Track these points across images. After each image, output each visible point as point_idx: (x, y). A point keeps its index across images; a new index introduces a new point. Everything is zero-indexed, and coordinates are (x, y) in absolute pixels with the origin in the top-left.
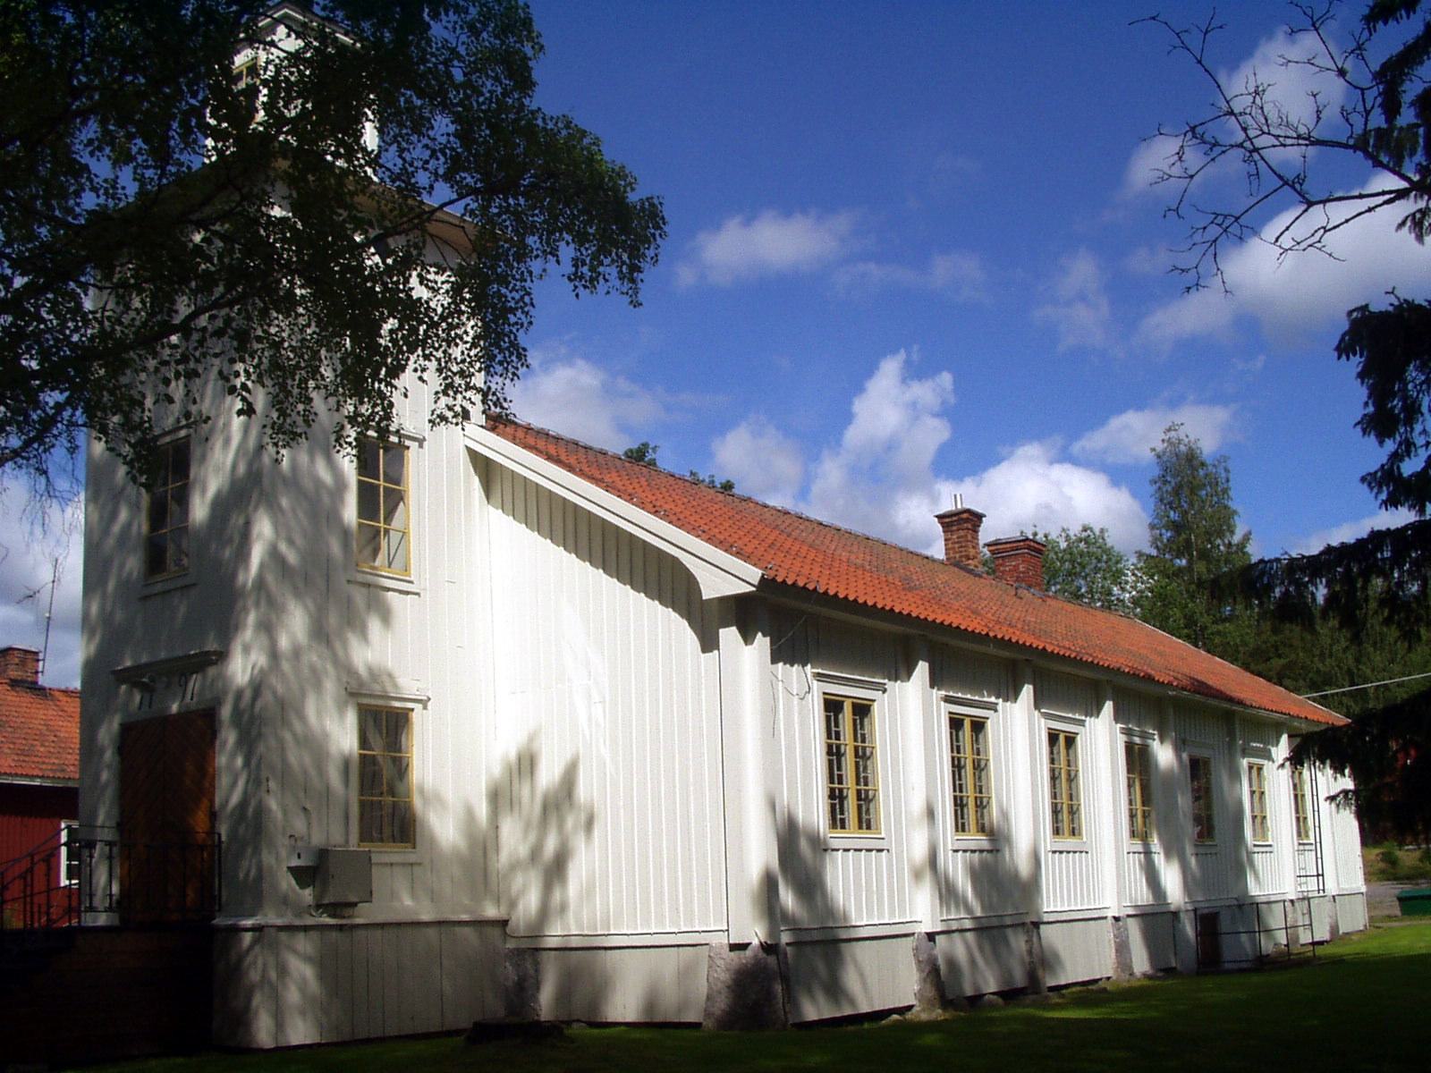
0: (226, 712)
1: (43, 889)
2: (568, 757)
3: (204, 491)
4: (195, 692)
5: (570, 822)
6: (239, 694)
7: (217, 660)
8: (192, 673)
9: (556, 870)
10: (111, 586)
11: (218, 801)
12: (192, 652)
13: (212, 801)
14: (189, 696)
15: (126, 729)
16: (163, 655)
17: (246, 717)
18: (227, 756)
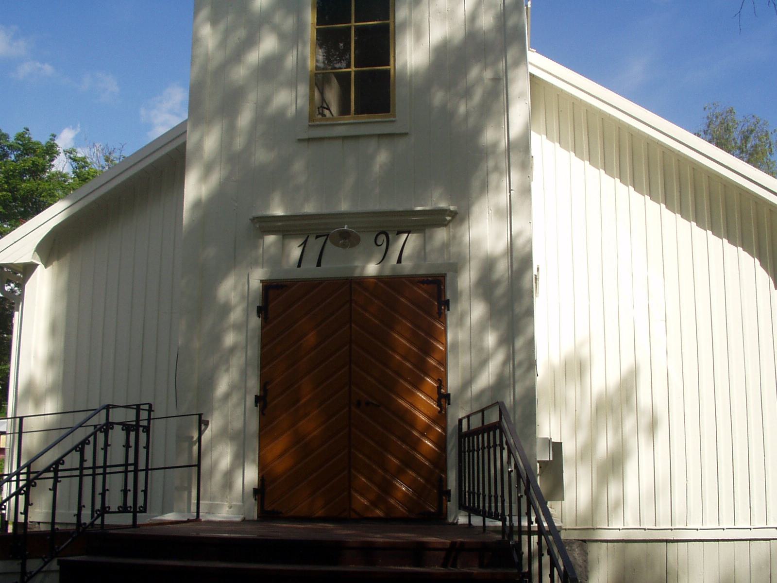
0: (467, 279)
1: (129, 473)
2: (627, 364)
3: (419, 36)
4: (406, 253)
5: (629, 424)
6: (489, 265)
7: (450, 221)
8: (400, 233)
9: (613, 466)
10: (245, 119)
11: (453, 381)
12: (419, 208)
13: (442, 382)
14: (394, 260)
15: (270, 288)
16: (344, 207)
17: (500, 291)
18: (468, 327)
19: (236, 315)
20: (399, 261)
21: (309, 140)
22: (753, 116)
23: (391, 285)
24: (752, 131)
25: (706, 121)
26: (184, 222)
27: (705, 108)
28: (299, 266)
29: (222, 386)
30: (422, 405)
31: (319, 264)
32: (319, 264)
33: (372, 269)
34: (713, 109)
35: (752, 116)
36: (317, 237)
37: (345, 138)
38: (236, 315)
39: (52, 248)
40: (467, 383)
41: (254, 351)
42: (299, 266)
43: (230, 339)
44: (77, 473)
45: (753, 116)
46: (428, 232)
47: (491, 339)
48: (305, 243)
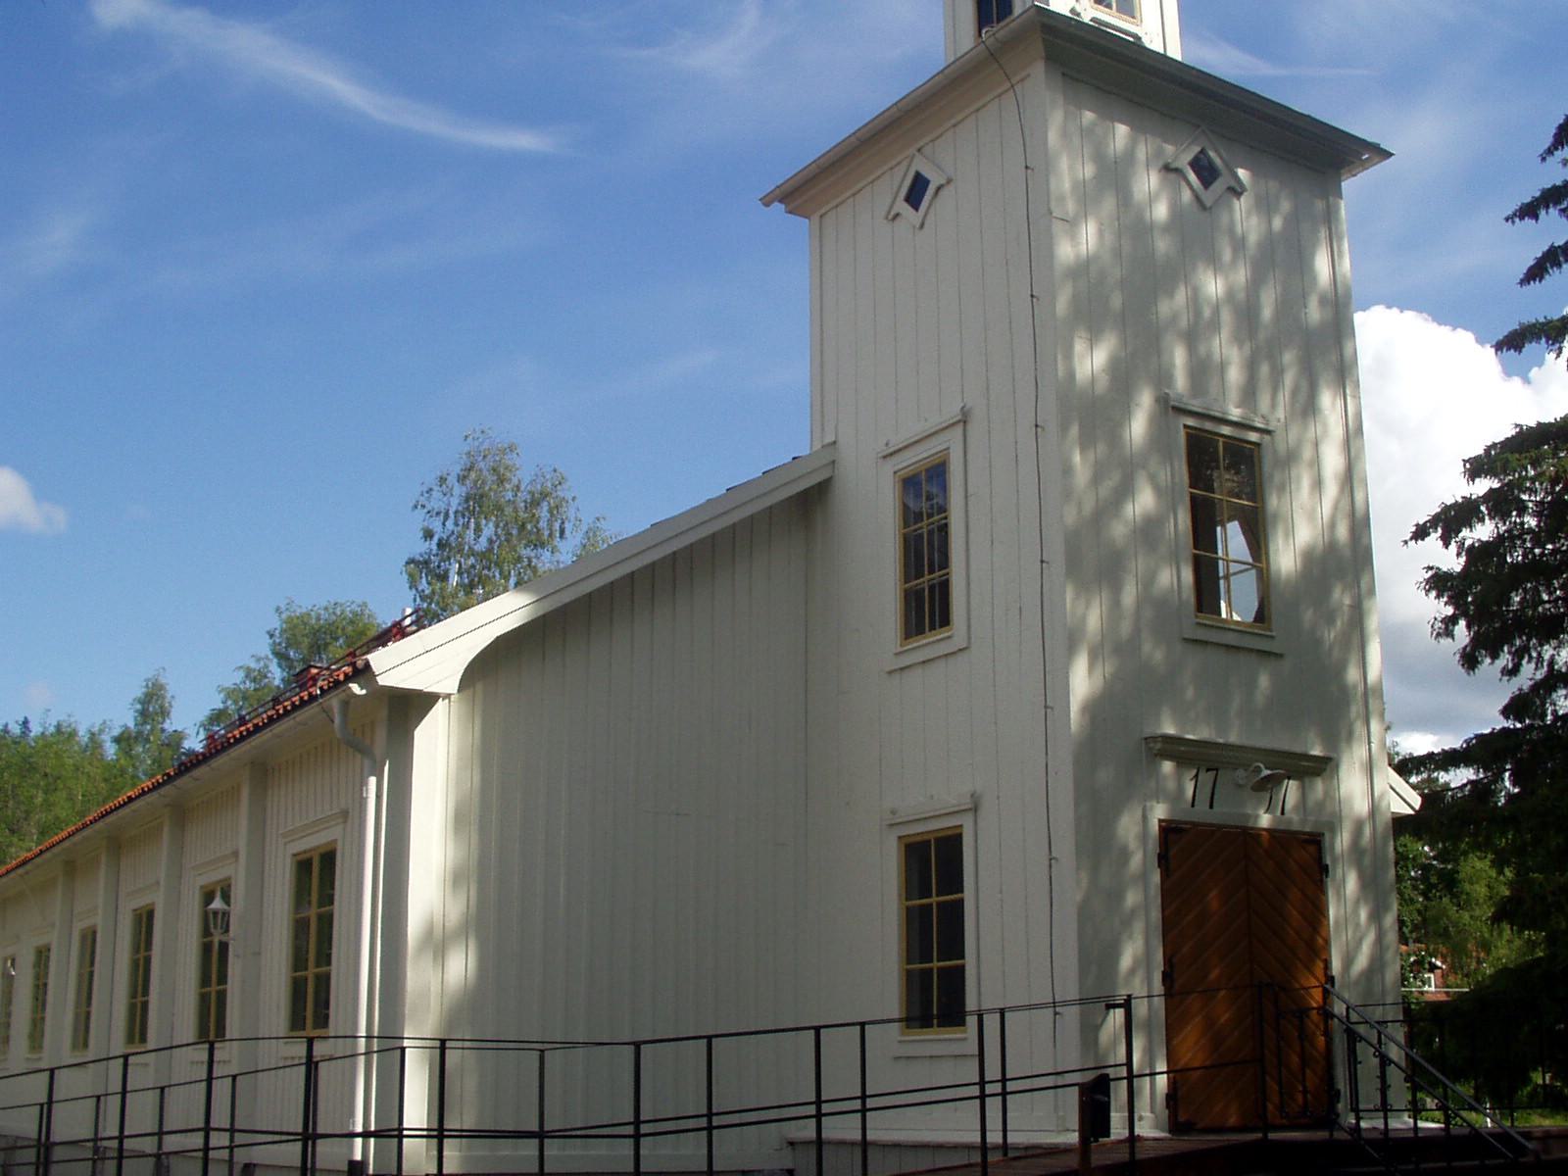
0: (1342, 841)
19: (1136, 861)
20: (1283, 813)
21: (1196, 641)
22: (555, 471)
23: (1283, 839)
24: (544, 495)
25: (465, 460)
26: (1072, 727)
27: (466, 437)
28: (1193, 806)
29: (1126, 961)
30: (1312, 983)
31: (1211, 807)
32: (1211, 807)
33: (1265, 820)
34: (480, 440)
35: (552, 469)
36: (1208, 770)
37: (1228, 647)
38: (1136, 861)
39: (488, 668)
40: (1348, 961)
41: (1156, 915)
42: (1193, 806)
43: (1132, 898)
44: (825, 1108)
45: (555, 471)
46: (1307, 780)
47: (1363, 914)
48: (1196, 776)
